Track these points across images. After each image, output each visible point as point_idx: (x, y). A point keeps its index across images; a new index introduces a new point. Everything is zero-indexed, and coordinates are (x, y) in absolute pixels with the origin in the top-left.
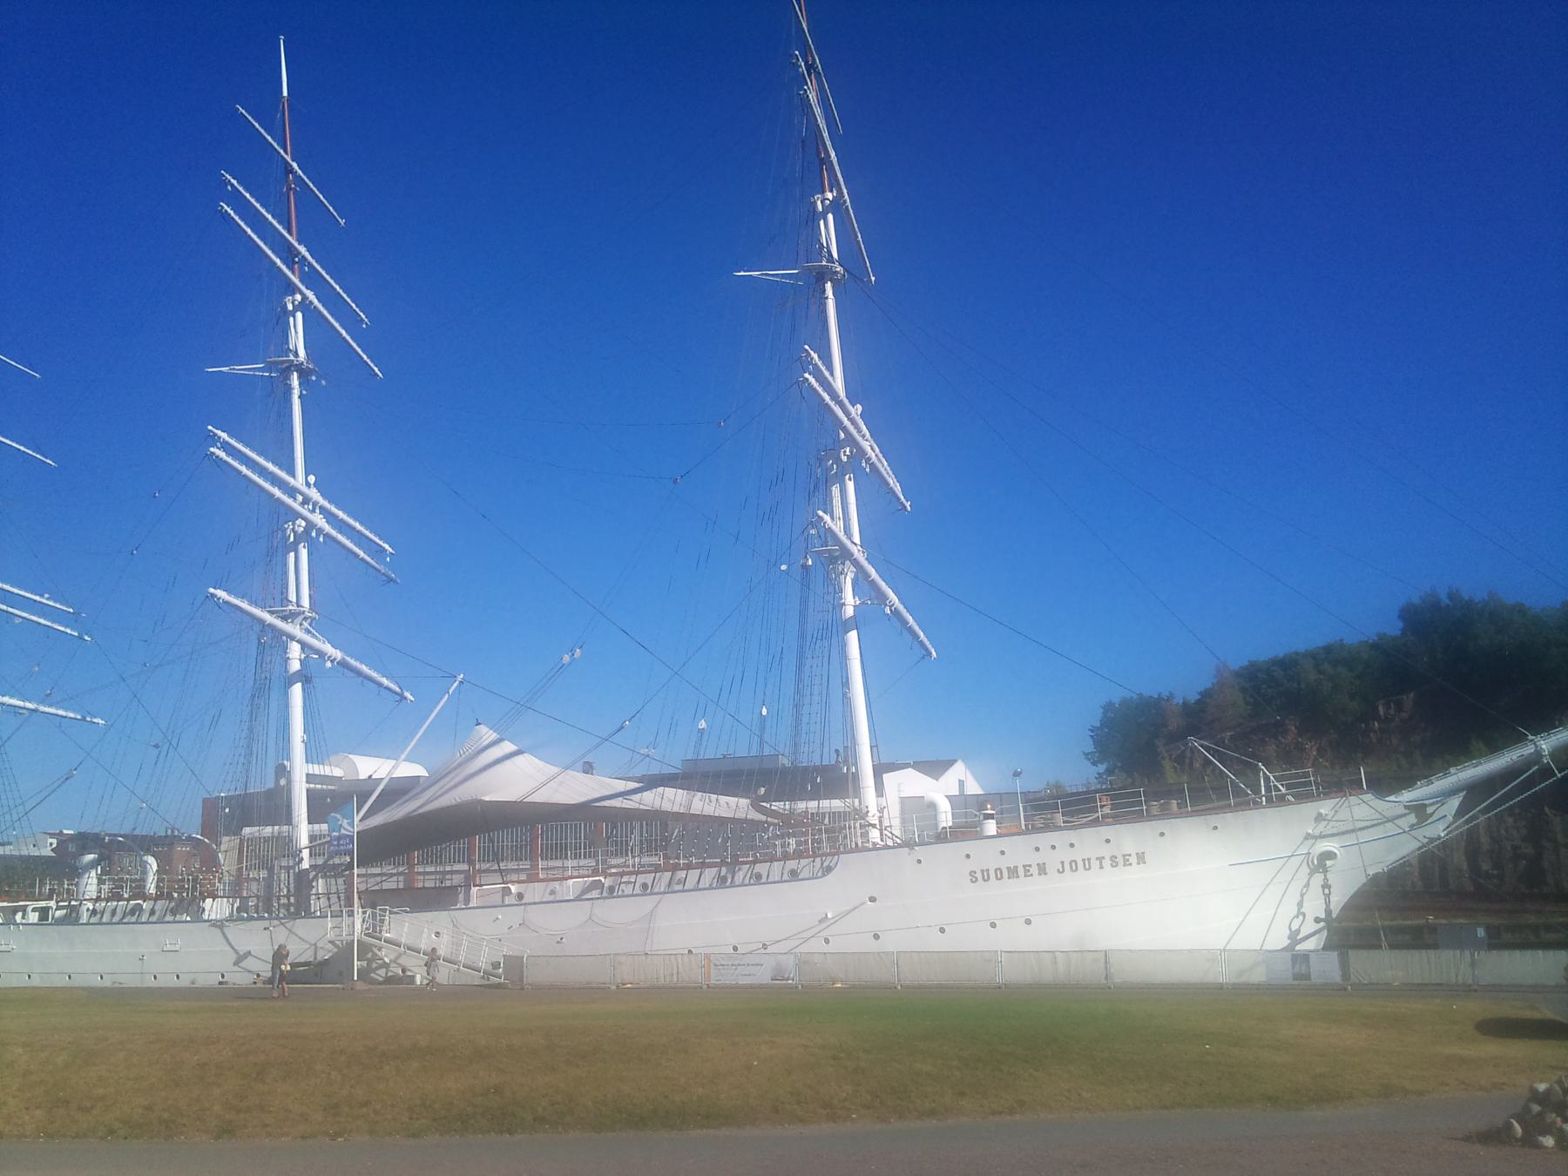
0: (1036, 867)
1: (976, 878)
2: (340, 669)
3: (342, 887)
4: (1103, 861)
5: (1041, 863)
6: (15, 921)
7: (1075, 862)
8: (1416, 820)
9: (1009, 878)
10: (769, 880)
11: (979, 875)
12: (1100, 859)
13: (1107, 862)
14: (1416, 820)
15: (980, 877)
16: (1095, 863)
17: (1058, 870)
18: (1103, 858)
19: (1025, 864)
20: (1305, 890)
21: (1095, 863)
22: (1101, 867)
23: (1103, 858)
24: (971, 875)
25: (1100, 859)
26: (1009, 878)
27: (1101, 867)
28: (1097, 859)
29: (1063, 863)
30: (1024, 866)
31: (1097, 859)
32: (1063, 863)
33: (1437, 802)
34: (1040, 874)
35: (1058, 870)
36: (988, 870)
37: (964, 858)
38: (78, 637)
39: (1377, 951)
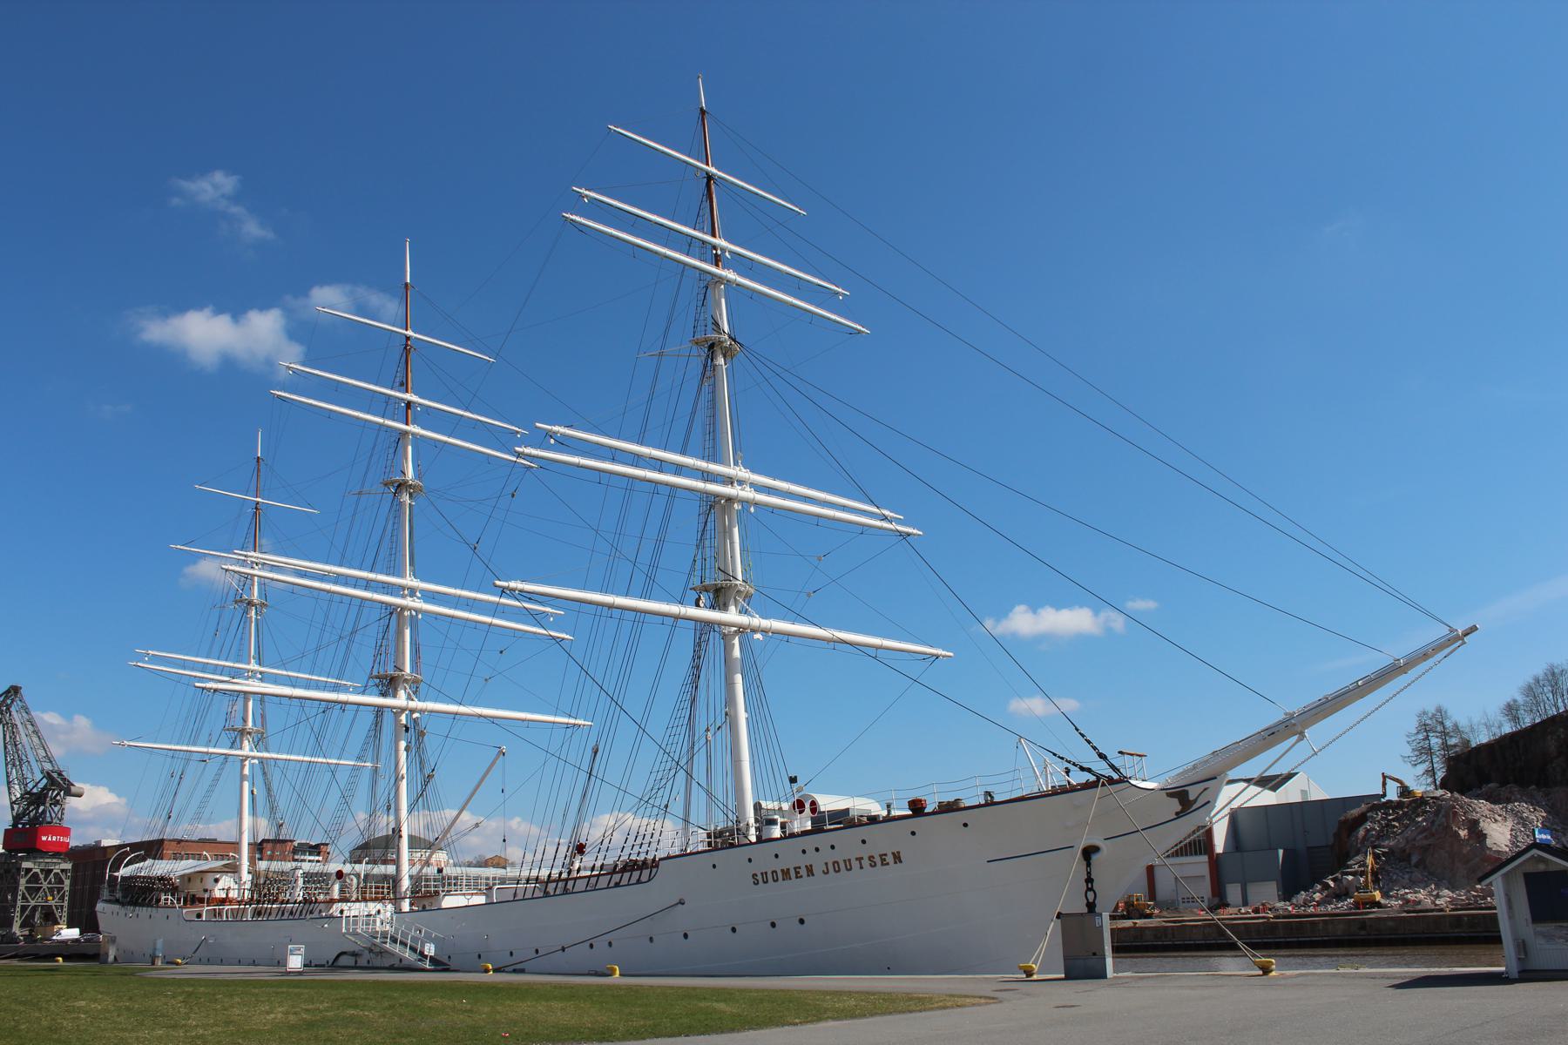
0: (805, 869)
1: (875, 863)
2: (250, 511)
3: (700, 849)
4: (862, 861)
5: (808, 864)
6: (1094, 782)
7: (837, 863)
8: (1180, 807)
9: (784, 880)
10: (535, 896)
11: (878, 860)
12: (860, 859)
13: (866, 862)
14: (1180, 807)
15: (760, 880)
16: (855, 864)
17: (823, 871)
18: (862, 858)
19: (881, 853)
20: (1091, 895)
21: (855, 864)
22: (861, 868)
23: (862, 858)
24: (753, 878)
25: (860, 859)
26: (784, 880)
27: (861, 868)
28: (857, 859)
29: (826, 864)
30: (795, 868)
31: (857, 859)
32: (826, 864)
33: (245, 622)
34: (896, 863)
35: (823, 871)
36: (766, 873)
37: (780, 856)
38: (406, 284)
39: (1102, 980)
